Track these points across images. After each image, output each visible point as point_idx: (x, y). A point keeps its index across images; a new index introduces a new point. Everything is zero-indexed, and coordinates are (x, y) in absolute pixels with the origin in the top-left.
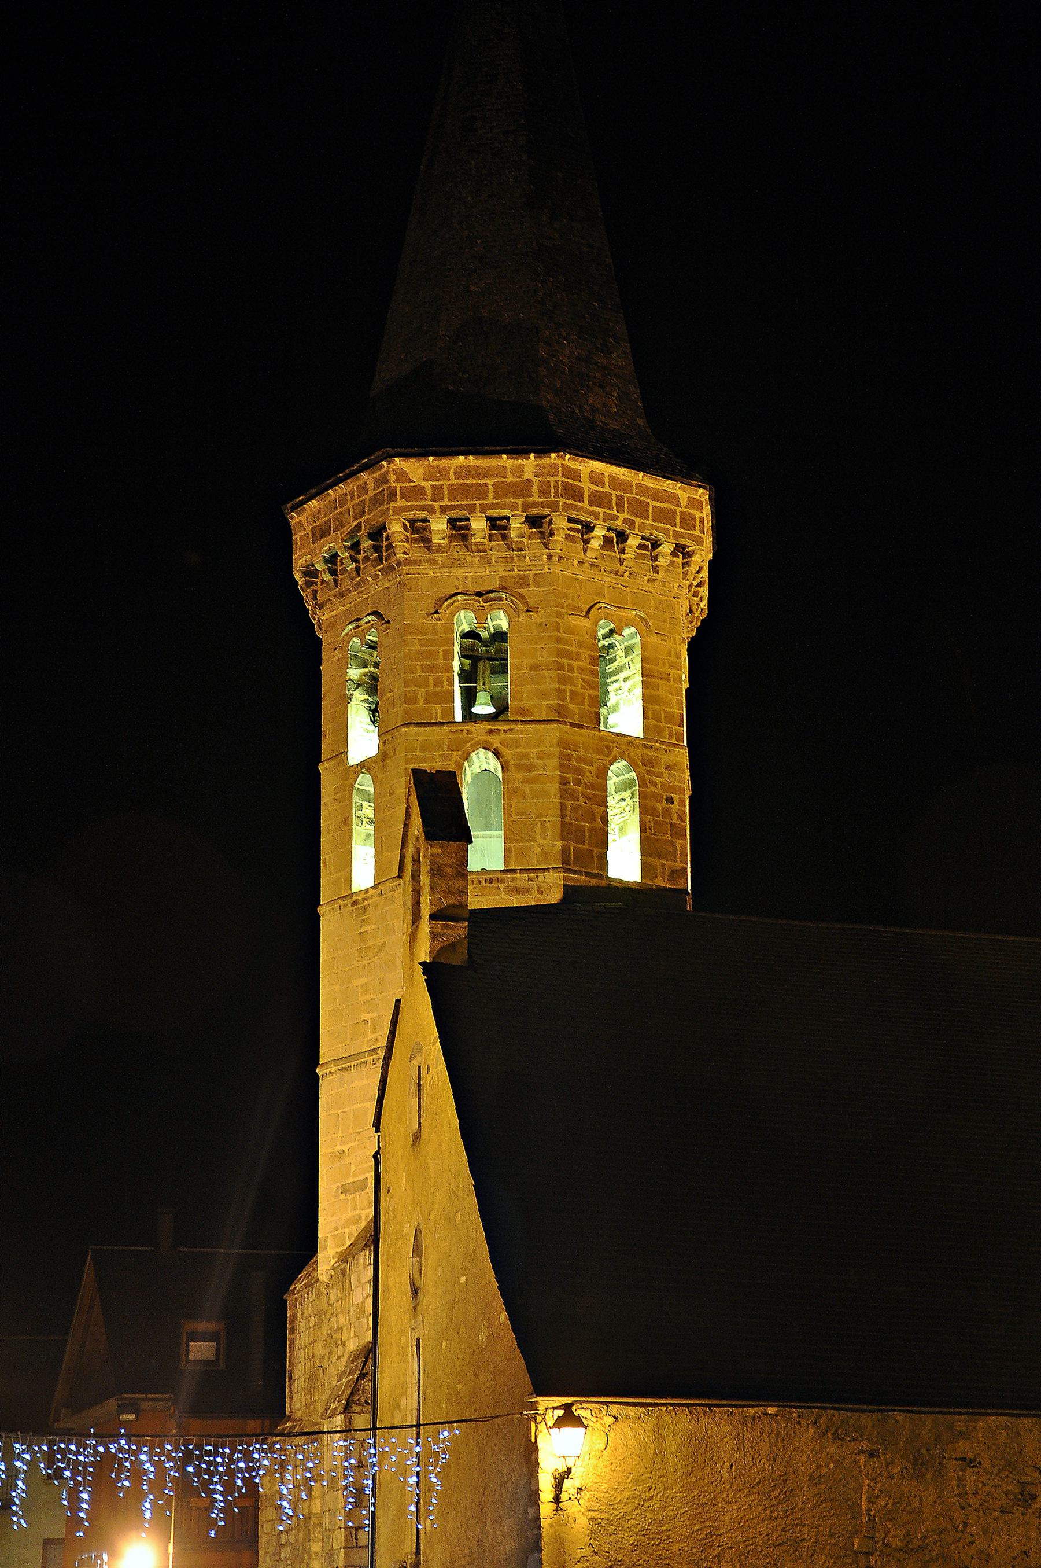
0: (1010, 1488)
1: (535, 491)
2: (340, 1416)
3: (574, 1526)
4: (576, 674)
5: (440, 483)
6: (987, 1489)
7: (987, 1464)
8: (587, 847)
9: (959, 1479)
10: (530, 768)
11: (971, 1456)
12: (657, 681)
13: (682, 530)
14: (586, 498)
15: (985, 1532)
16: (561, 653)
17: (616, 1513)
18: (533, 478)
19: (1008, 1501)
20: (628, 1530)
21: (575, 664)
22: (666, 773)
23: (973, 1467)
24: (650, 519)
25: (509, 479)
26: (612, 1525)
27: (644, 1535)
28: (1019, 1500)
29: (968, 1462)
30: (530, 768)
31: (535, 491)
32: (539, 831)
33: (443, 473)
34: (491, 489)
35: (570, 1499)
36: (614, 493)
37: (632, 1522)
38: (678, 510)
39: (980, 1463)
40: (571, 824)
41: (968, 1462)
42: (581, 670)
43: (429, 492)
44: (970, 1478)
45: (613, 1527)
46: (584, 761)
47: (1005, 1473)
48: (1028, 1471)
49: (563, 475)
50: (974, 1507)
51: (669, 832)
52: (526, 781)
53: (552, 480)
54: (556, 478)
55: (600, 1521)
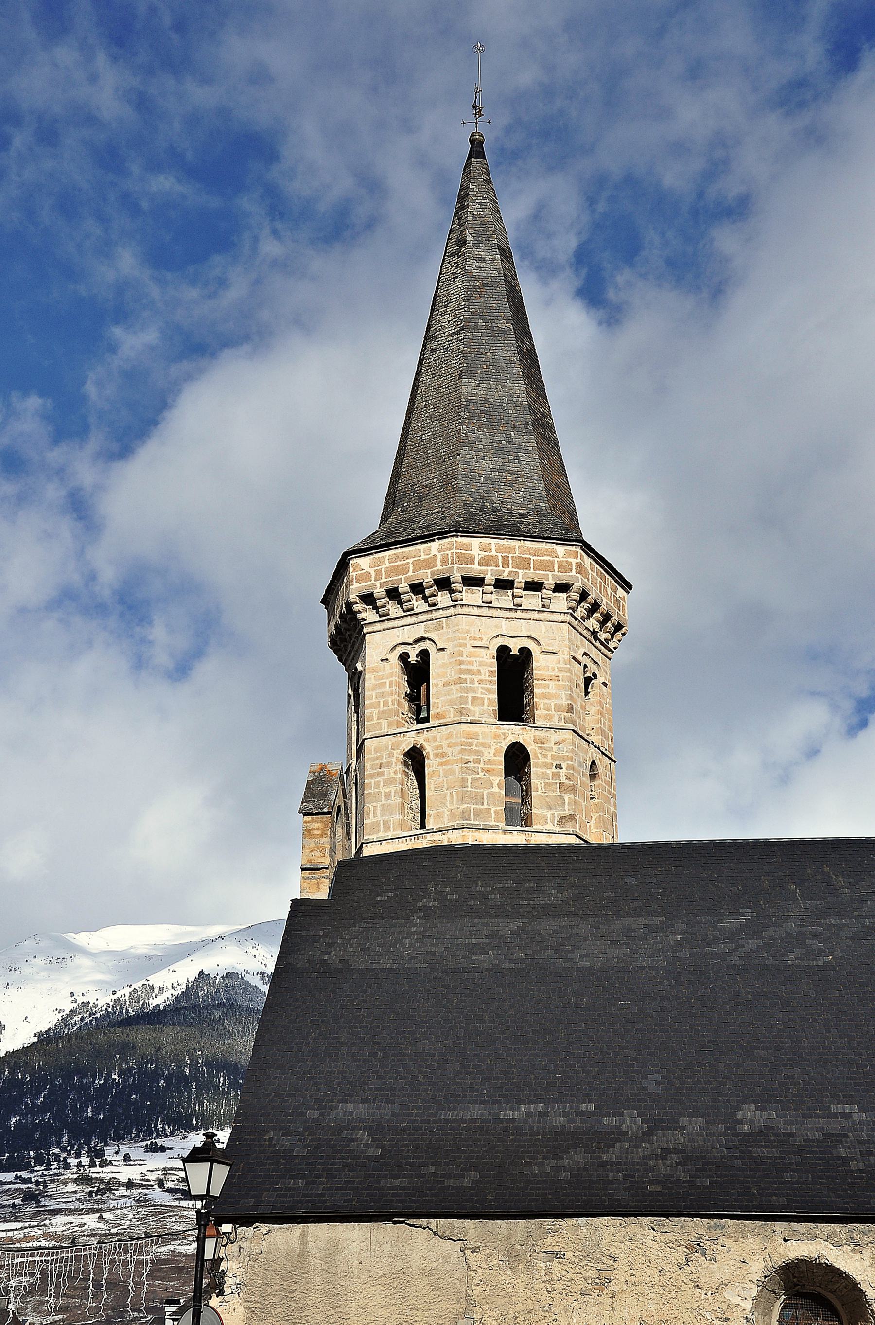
0: (588, 1274)
1: (439, 562)
2: (215, 1239)
3: (233, 1314)
4: (477, 684)
5: (380, 567)
6: (569, 1276)
7: (569, 1255)
8: (485, 806)
9: (548, 1268)
10: (443, 755)
11: (557, 1249)
12: (547, 682)
13: (560, 573)
14: (476, 562)
15: (566, 1311)
16: (462, 672)
17: (267, 1302)
18: (437, 554)
19: (587, 1285)
20: (275, 1316)
21: (476, 678)
22: (555, 748)
23: (559, 1258)
24: (532, 569)
25: (423, 557)
26: (263, 1312)
27: (287, 1320)
28: (597, 1284)
29: (557, 1255)
30: (443, 755)
31: (439, 562)
32: (448, 798)
33: (381, 562)
34: (411, 566)
35: (232, 1293)
36: (500, 555)
37: (279, 1310)
38: (556, 559)
39: (564, 1255)
40: (472, 791)
41: (557, 1255)
42: (480, 682)
43: (373, 574)
44: (557, 1268)
45: (264, 1315)
46: (483, 745)
47: (585, 1262)
48: (605, 1260)
49: (457, 549)
50: (558, 1291)
51: (558, 790)
52: (441, 764)
53: (449, 553)
54: (452, 551)
55: (254, 1309)
